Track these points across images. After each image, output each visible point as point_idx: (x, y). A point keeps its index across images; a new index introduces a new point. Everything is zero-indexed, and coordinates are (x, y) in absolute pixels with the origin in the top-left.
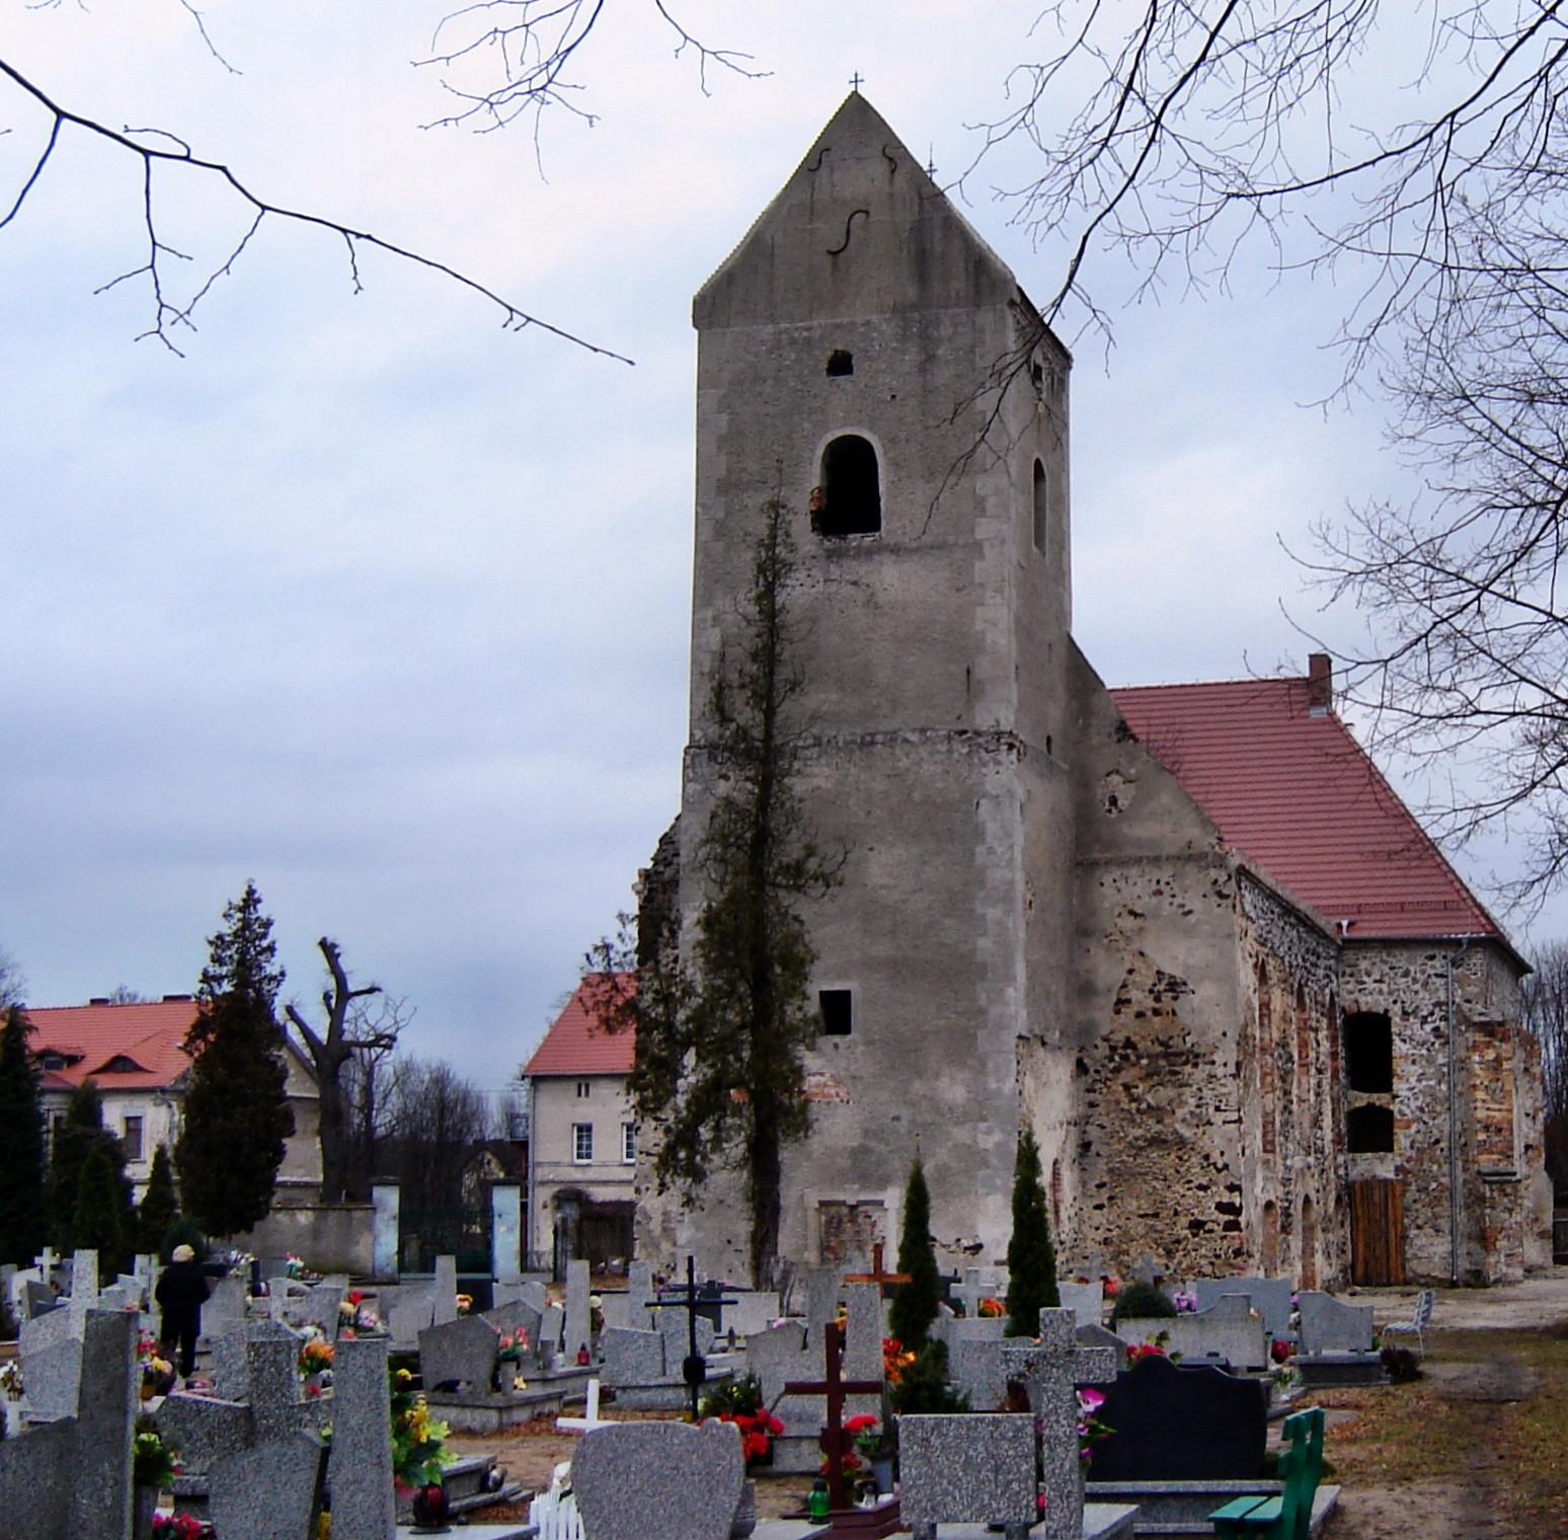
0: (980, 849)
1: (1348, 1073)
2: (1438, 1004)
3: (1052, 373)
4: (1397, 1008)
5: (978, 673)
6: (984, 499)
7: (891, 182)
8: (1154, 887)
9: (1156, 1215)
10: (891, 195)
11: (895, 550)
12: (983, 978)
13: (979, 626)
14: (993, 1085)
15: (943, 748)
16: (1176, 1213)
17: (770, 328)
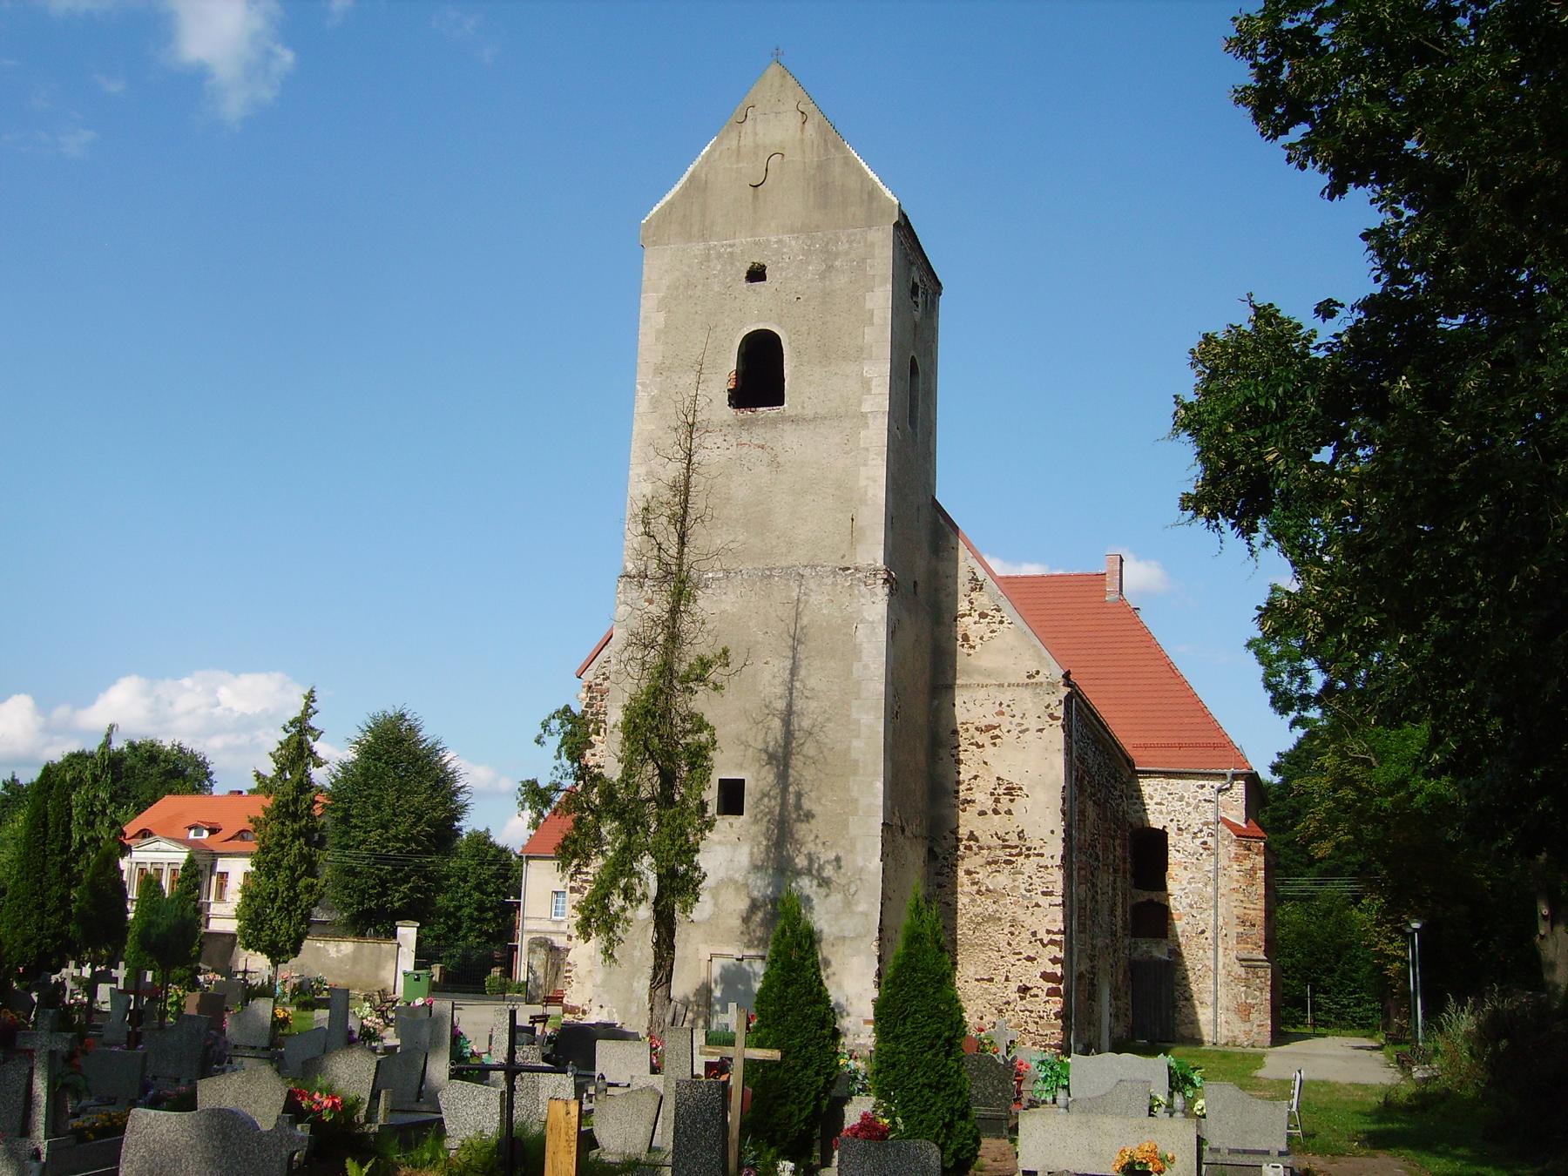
0: (856, 666)
1: (1133, 875)
2: (1206, 824)
3: (925, 293)
4: (1174, 825)
5: (859, 522)
6: (870, 379)
7: (802, 130)
8: (998, 709)
9: (991, 980)
10: (802, 140)
11: (793, 420)
12: (855, 773)
13: (862, 483)
14: (860, 863)
15: (829, 581)
16: (1007, 979)
17: (701, 245)
